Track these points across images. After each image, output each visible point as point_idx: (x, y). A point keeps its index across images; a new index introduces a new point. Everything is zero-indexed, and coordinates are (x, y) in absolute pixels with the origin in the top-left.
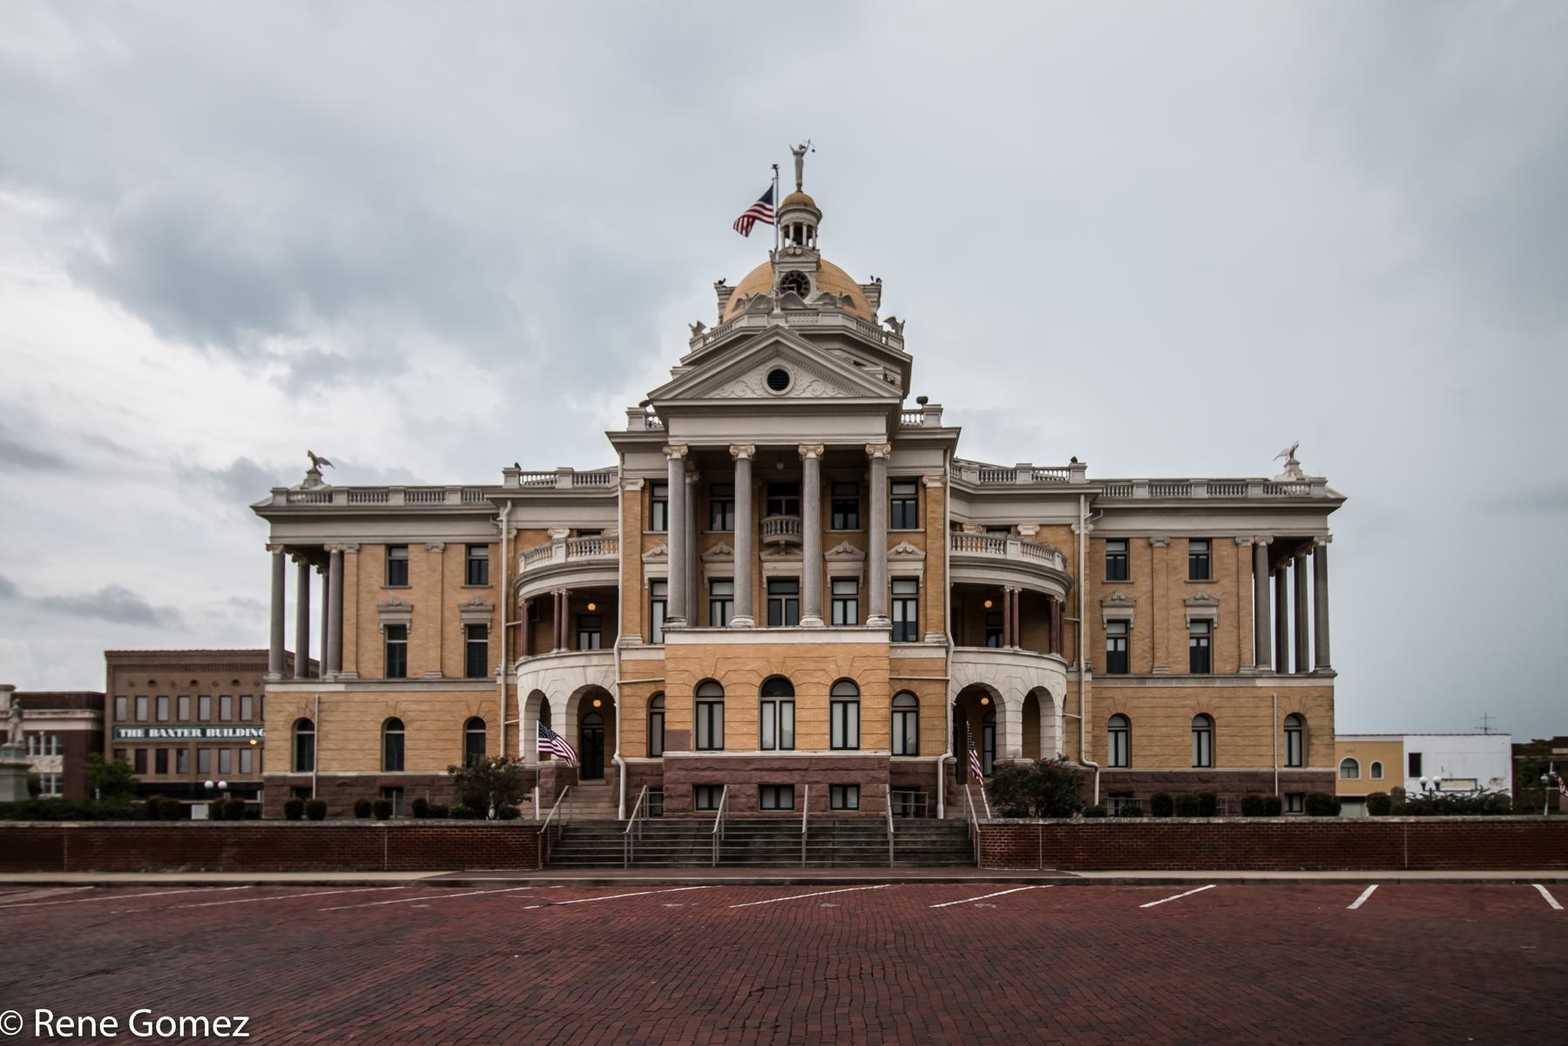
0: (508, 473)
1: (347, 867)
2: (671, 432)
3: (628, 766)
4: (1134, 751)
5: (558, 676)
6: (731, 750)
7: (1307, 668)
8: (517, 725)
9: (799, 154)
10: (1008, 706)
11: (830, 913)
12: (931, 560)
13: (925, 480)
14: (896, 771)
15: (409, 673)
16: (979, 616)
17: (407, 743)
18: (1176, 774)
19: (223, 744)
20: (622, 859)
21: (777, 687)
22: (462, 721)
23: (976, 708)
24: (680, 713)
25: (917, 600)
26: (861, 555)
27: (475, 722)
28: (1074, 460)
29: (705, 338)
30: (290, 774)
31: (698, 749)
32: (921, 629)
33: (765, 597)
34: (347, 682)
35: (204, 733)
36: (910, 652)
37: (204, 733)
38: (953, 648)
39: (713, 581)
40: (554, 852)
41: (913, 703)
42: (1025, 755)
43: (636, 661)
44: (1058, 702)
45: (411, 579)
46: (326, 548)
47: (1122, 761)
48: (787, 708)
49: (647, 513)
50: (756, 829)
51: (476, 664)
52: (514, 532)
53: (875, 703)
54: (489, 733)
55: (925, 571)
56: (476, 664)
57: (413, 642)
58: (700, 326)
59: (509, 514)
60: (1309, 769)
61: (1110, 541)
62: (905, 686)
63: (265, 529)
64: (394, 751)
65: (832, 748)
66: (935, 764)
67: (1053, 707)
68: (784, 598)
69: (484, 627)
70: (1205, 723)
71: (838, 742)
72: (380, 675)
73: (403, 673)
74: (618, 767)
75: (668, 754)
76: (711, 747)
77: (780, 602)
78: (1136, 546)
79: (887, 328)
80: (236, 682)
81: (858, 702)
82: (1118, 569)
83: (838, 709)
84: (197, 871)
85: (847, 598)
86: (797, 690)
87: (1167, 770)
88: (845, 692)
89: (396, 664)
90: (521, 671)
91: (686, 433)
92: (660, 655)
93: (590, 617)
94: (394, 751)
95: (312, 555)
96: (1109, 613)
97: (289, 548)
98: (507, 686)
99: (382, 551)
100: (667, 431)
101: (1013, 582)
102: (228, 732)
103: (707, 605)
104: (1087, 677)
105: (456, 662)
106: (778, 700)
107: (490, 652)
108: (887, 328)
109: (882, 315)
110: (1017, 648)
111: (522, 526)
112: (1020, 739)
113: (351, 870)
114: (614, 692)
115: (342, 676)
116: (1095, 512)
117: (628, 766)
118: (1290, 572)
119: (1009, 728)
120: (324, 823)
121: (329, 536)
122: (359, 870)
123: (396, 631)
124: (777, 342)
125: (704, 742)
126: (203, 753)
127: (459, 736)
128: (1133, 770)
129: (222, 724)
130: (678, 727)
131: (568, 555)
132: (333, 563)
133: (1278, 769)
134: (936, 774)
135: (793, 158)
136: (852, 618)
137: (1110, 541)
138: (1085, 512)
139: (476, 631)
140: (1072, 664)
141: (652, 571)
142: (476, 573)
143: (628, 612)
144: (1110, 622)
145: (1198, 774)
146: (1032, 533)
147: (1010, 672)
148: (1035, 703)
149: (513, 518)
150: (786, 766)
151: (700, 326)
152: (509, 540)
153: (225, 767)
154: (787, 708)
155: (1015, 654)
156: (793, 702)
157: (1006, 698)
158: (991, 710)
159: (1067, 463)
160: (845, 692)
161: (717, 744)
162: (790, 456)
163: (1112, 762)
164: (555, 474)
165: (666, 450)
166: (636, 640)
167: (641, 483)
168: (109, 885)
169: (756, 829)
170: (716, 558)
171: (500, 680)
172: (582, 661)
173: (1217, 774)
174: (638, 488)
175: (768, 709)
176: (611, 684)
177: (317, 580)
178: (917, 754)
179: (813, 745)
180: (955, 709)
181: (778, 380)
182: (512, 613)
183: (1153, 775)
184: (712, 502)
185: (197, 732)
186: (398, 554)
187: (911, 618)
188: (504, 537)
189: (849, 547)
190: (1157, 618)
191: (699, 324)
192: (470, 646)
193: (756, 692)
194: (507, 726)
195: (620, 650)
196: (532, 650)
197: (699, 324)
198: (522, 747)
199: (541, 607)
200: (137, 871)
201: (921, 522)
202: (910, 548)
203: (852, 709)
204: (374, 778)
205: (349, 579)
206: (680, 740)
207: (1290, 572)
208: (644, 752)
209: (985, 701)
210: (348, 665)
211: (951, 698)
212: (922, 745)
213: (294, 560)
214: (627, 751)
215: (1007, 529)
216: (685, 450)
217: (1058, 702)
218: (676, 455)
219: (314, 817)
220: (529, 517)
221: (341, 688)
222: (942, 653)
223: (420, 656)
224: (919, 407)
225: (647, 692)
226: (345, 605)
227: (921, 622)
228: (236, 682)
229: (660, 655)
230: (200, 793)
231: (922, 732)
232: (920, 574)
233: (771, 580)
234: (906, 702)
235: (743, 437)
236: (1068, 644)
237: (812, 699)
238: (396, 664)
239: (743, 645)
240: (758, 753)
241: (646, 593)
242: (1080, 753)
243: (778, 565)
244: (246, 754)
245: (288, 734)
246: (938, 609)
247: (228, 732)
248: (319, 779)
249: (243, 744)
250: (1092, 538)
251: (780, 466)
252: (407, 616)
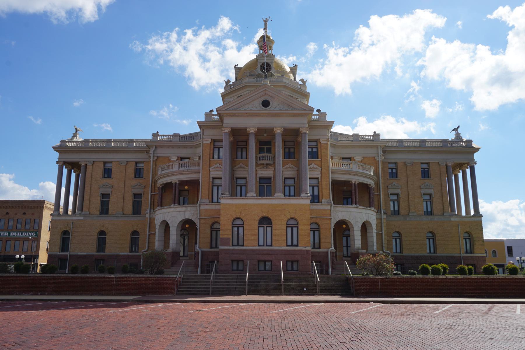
0: (154, 135)
1: (99, 293)
2: (225, 121)
3: (202, 252)
4: (404, 247)
5: (174, 215)
6: (247, 246)
7: (470, 213)
8: (155, 234)
9: (266, 22)
10: (355, 229)
11: (274, 315)
12: (324, 171)
13: (321, 141)
14: (314, 256)
15: (110, 212)
16: (345, 192)
17: (107, 241)
18: (421, 256)
19: (16, 239)
20: (209, 291)
21: (265, 221)
22: (130, 233)
23: (342, 229)
24: (225, 231)
25: (318, 186)
26: (296, 169)
27: (135, 233)
28: (375, 132)
29: (231, 85)
30: (59, 253)
31: (233, 246)
32: (320, 198)
33: (258, 185)
34: (85, 216)
35: (9, 234)
36: (316, 207)
37: (9, 234)
38: (333, 205)
39: (237, 178)
40: (179, 288)
41: (317, 227)
42: (362, 249)
43: (206, 210)
44: (374, 227)
45: (113, 175)
46: (80, 163)
47: (399, 251)
48: (269, 229)
49: (212, 152)
50: (261, 279)
51: (137, 210)
52: (156, 158)
53: (305, 228)
54: (141, 237)
55: (321, 176)
56: (137, 210)
57: (112, 200)
58: (229, 81)
59: (154, 151)
60: (474, 255)
61: (389, 163)
62: (314, 220)
63: (57, 154)
64: (101, 242)
65: (287, 246)
66: (327, 252)
67: (372, 229)
68: (265, 185)
69: (141, 195)
70: (432, 237)
71: (290, 243)
72: (98, 213)
73: (107, 213)
74: (198, 253)
75: (222, 248)
76: (238, 245)
77: (265, 187)
78: (400, 166)
79: (300, 83)
80: (24, 213)
81: (298, 227)
82: (394, 175)
83: (289, 230)
84: (37, 294)
85: (294, 188)
86: (273, 222)
87: (417, 254)
88: (293, 224)
89: (104, 209)
90: (156, 213)
91: (230, 123)
92: (217, 207)
93: (184, 192)
94: (101, 242)
95: (73, 166)
96: (391, 191)
97: (65, 163)
98: (150, 218)
99: (102, 165)
100: (222, 122)
101: (355, 179)
102: (19, 234)
103: (237, 188)
104: (384, 217)
105: (129, 208)
106: (265, 226)
107: (143, 204)
108: (300, 83)
109: (298, 79)
110: (358, 205)
111: (159, 155)
112: (360, 242)
113: (99, 295)
114: (197, 222)
115: (83, 214)
116: (384, 152)
117: (202, 252)
118: (460, 175)
119: (356, 237)
120: (87, 275)
121: (81, 159)
122: (102, 295)
123: (105, 196)
124: (265, 90)
125: (235, 243)
126: (8, 243)
127: (128, 238)
128: (404, 254)
129: (17, 230)
130: (225, 237)
131: (179, 168)
132: (82, 169)
133: (462, 255)
134: (328, 256)
135: (264, 23)
136: (292, 193)
137: (389, 163)
138: (381, 153)
139: (137, 196)
140: (379, 211)
141: (214, 174)
142: (138, 173)
143: (203, 190)
144: (391, 194)
145: (430, 256)
146: (360, 160)
147: (357, 215)
148: (365, 227)
149: (155, 152)
150: (270, 253)
151: (229, 81)
152: (153, 161)
153: (25, 249)
154: (269, 229)
155: (357, 208)
156: (272, 227)
157: (354, 225)
158: (348, 229)
159: (372, 134)
160: (293, 224)
161: (241, 243)
162: (270, 131)
163: (395, 251)
164: (172, 136)
165: (223, 129)
166: (206, 201)
167: (210, 141)
168: (8, 300)
169: (261, 279)
170: (239, 169)
171: (148, 216)
172: (184, 209)
173: (438, 256)
174: (209, 142)
175: (261, 229)
176: (195, 219)
177: (73, 175)
178: (319, 248)
179: (280, 245)
180: (334, 229)
181: (266, 104)
182: (153, 190)
183: (412, 257)
184: (237, 148)
185: (6, 234)
186: (108, 166)
187: (316, 193)
188: (152, 159)
189: (291, 166)
190: (410, 193)
191: (228, 80)
192: (134, 202)
193: (257, 223)
194: (149, 234)
195: (200, 205)
196: (161, 205)
197: (228, 80)
198: (156, 243)
199: (167, 186)
200: (13, 294)
201: (319, 156)
202: (315, 166)
203: (295, 230)
204: (93, 255)
205: (88, 175)
206: (225, 242)
207: (460, 175)
208: (209, 247)
209: (344, 226)
210: (85, 209)
211: (332, 227)
212: (322, 244)
213: (66, 168)
214: (202, 245)
215: (350, 159)
216: (230, 129)
217: (374, 227)
218: (226, 131)
219: (83, 273)
220: (161, 152)
221: (82, 218)
222: (329, 207)
223: (114, 206)
224: (318, 113)
225: (211, 222)
226: (86, 185)
227: (320, 195)
228: (24, 213)
229: (217, 207)
230: (12, 259)
231: (299, 236)
232: (319, 176)
233: (260, 178)
234: (316, 228)
235: (252, 125)
236: (376, 203)
237: (279, 225)
238: (104, 209)
239: (253, 203)
240: (258, 248)
241: (211, 183)
242: (382, 247)
243: (263, 172)
244: (26, 243)
245: (59, 237)
246: (327, 191)
247: (19, 234)
248: (70, 255)
249: (26, 239)
250: (383, 162)
251: (265, 135)
252: (111, 190)
